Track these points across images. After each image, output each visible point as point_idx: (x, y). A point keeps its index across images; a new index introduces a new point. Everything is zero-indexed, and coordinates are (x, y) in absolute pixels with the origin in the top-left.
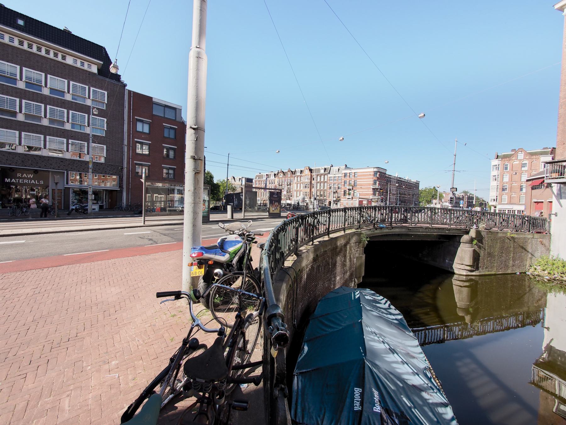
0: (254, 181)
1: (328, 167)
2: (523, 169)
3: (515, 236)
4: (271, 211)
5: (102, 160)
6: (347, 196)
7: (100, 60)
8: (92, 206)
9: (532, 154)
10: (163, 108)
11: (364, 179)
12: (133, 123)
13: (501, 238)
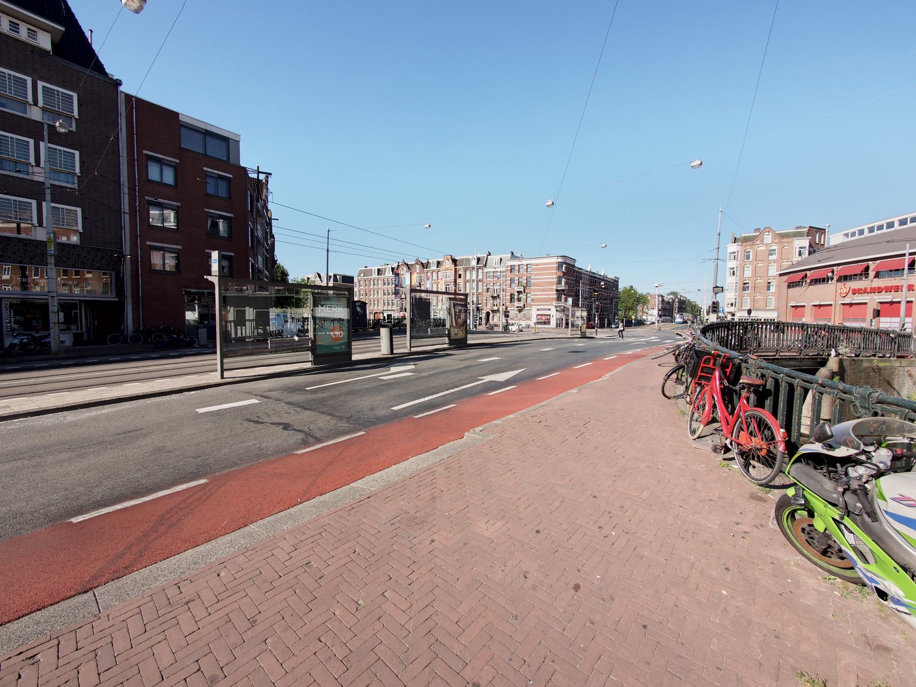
0: (355, 280)
1: (483, 255)
2: (771, 258)
3: (881, 365)
4: (453, 337)
5: (75, 239)
6: (516, 304)
7: (60, 24)
8: (59, 338)
9: (783, 236)
10: (201, 136)
11: (542, 274)
12: (139, 163)
13: (865, 369)
